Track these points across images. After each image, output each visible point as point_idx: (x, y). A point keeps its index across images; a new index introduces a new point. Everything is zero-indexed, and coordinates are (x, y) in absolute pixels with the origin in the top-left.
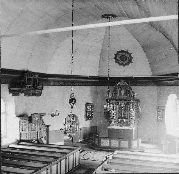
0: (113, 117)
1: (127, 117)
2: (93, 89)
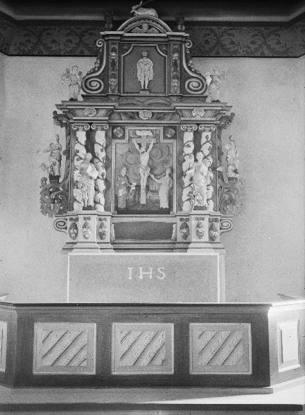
0: (92, 203)
1: (164, 204)
2: (278, 386)
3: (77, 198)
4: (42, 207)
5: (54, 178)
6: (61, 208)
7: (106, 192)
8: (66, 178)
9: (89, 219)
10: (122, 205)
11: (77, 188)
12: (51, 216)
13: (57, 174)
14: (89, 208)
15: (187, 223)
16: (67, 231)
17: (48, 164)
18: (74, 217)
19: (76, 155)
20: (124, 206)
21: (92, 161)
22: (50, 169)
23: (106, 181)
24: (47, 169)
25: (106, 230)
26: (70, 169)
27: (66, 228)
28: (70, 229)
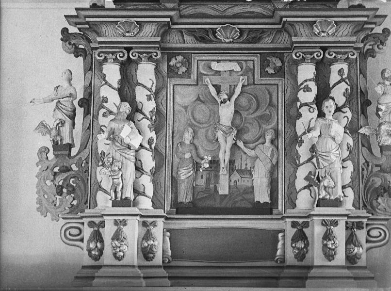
0: (129, 194)
3: (103, 185)
4: (39, 202)
5: (62, 148)
6: (75, 202)
7: (155, 173)
8: (84, 146)
9: (124, 223)
10: (185, 197)
11: (103, 165)
13: (67, 140)
15: (101, 230)
16: (84, 245)
17: (51, 123)
18: (97, 220)
21: (130, 118)
22: (54, 132)
24: (49, 132)
25: (156, 243)
26: (90, 132)
27: (82, 240)
28: (90, 241)
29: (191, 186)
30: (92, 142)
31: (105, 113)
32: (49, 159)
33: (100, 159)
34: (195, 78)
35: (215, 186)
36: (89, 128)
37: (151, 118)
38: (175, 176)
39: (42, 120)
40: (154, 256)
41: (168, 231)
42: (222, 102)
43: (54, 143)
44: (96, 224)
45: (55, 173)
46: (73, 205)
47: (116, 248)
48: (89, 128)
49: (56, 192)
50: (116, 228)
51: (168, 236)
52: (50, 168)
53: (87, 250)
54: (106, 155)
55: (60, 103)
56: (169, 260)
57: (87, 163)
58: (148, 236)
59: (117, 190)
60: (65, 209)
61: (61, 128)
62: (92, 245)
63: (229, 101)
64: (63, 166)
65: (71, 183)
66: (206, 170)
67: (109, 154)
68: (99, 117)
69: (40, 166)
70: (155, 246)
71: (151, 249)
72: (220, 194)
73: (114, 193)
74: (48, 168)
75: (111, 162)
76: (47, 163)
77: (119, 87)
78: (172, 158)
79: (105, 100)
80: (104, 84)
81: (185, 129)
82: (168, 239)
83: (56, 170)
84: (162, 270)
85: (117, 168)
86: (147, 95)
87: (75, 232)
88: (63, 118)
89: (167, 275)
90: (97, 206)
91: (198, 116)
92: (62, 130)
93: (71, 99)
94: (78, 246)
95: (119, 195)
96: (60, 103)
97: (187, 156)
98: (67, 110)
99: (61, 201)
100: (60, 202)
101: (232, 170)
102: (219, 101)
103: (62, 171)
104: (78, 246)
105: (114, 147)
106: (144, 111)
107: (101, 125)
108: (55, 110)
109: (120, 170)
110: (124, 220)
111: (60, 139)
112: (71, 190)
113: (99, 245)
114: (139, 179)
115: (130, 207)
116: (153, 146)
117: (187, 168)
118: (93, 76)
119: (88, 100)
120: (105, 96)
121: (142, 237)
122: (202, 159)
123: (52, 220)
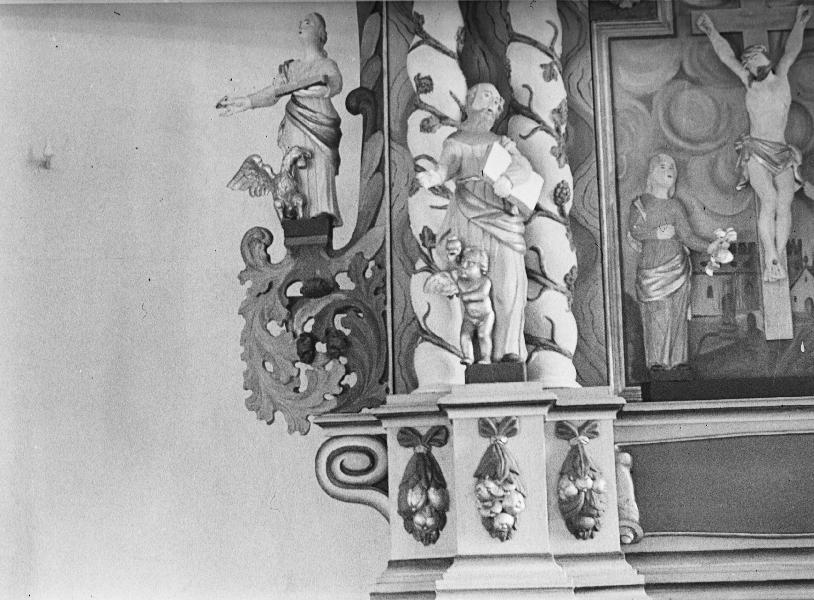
0: (515, 345)
3: (434, 324)
4: (251, 383)
5: (307, 229)
6: (352, 380)
7: (577, 283)
8: (368, 221)
9: (509, 427)
10: (666, 351)
11: (430, 268)
12: (299, 427)
13: (320, 206)
14: (508, 369)
15: (436, 451)
16: (390, 503)
17: (276, 161)
18: (423, 426)
19: (415, 104)
20: (680, 356)
21: (500, 129)
22: (284, 185)
23: (575, 225)
24: (272, 183)
25: (601, 484)
26: (385, 184)
27: (382, 485)
28: (405, 485)
29: (683, 318)
30: (391, 208)
31: (427, 120)
32: (272, 261)
33: (418, 250)
34: (669, 18)
35: (751, 318)
36: (380, 169)
37: (558, 130)
38: (633, 293)
39: (248, 153)
40: (598, 523)
41: (624, 449)
42: (753, 78)
43: (285, 216)
44: (420, 436)
45: (293, 300)
46: (346, 388)
47: (489, 504)
48: (380, 169)
49: (298, 354)
50: (485, 443)
51: (626, 465)
52: (277, 286)
53: (400, 512)
54: (438, 238)
55: (299, 105)
56: (635, 535)
57: (381, 266)
58: (574, 465)
59: (481, 335)
60: (325, 399)
61: (303, 173)
62: (414, 498)
63: (774, 73)
64: (315, 279)
65: (339, 326)
66: (722, 270)
67: (449, 232)
68: (410, 136)
69: (249, 284)
70: (599, 492)
71: (589, 504)
72: (769, 337)
73: (470, 343)
74: (271, 285)
75: (458, 253)
76: (268, 274)
77: (461, 49)
78: (620, 241)
79: (425, 84)
80: (419, 44)
81: (649, 161)
82: (626, 472)
83: (295, 290)
84: (623, 565)
85: (475, 271)
86: (542, 66)
87: (357, 461)
88: (309, 146)
89: (641, 580)
90: (416, 385)
91: (684, 122)
92: (305, 180)
93: (327, 91)
94: (370, 504)
95: (486, 349)
96: (299, 105)
97: (665, 233)
98: (316, 122)
99: (313, 378)
100: (311, 379)
101: (798, 269)
102: (743, 76)
103: (310, 293)
104: (370, 504)
105: (464, 209)
106: (535, 109)
107: (414, 156)
108: (283, 126)
109: (484, 275)
110: (507, 418)
111: (301, 203)
112: (340, 347)
113: (434, 497)
114: (538, 301)
115: (522, 380)
116: (568, 207)
117: (666, 268)
118: (384, 26)
119: (373, 93)
120: (423, 75)
121: (558, 468)
122: (710, 241)
123: (291, 431)
